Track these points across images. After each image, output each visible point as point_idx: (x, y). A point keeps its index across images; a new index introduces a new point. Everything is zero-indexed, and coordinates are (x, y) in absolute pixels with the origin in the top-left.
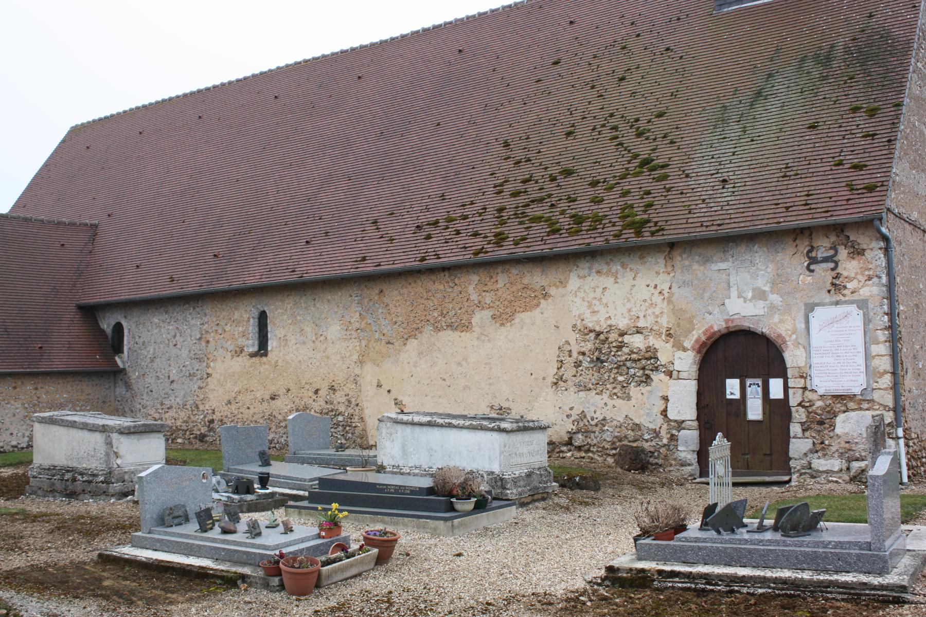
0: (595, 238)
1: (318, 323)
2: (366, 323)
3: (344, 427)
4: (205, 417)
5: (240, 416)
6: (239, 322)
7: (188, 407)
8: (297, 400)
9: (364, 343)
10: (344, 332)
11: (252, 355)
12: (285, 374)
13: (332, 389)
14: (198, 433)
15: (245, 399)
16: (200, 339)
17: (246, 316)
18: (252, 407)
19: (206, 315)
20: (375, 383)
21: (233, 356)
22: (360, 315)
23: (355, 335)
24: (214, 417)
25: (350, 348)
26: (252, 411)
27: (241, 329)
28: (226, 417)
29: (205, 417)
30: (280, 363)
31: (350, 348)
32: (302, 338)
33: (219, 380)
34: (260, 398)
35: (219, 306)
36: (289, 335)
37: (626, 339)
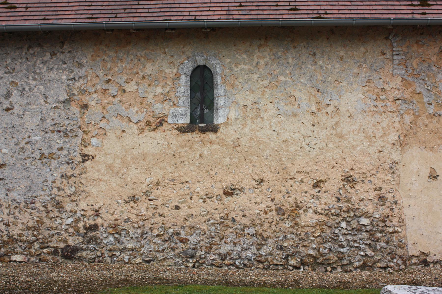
0: (195, 19)
1: (321, 87)
2: (414, 92)
3: (371, 234)
4: (77, 221)
5: (158, 219)
6: (162, 83)
7: (38, 205)
8: (279, 197)
9: (408, 119)
10: (371, 104)
11: (182, 130)
12: (254, 158)
13: (349, 180)
14: (62, 245)
15: (167, 195)
16: (67, 102)
17: (170, 71)
18: (184, 206)
19: (80, 65)
20: (426, 172)
21: (141, 131)
22: (403, 79)
23: (391, 106)
24: (99, 221)
25: (384, 125)
26: (184, 212)
27: (159, 90)
28: (126, 221)
29: (77, 221)
30: (244, 141)
31: (384, 125)
32: (290, 107)
33: (110, 167)
34: (202, 193)
35: (112, 54)
36: (263, 102)
37: (42, 93)
